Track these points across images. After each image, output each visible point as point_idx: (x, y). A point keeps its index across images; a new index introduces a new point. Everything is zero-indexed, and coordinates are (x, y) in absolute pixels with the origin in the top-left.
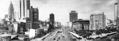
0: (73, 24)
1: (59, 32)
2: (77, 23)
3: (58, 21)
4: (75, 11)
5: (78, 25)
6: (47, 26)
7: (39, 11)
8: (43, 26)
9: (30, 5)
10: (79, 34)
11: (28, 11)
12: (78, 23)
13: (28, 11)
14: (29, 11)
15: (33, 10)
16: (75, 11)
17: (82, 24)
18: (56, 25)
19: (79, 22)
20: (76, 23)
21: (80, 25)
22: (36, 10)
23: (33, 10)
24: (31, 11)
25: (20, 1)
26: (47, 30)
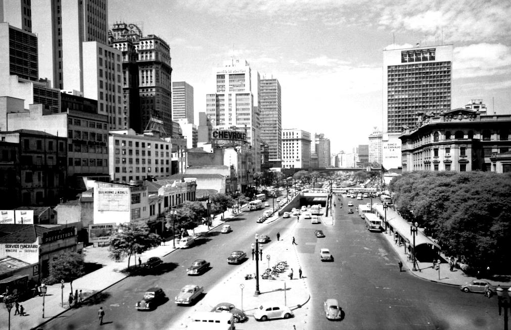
0: (410, 147)
1: (305, 202)
2: (431, 139)
3: (306, 130)
4: (431, 51)
5: (442, 152)
6: (227, 163)
7: (172, 54)
8: (200, 166)
9: (104, 17)
10: (237, 133)
11: (91, 48)
12: (442, 137)
13: (91, 48)
14: (100, 50)
15: (131, 46)
16: (431, 51)
17: (476, 145)
18: (292, 158)
19: (446, 129)
20: (424, 142)
21: (454, 153)
22: (150, 45)
23: (131, 46)
24: (109, 54)
25: (261, 260)
26: (218, 187)
